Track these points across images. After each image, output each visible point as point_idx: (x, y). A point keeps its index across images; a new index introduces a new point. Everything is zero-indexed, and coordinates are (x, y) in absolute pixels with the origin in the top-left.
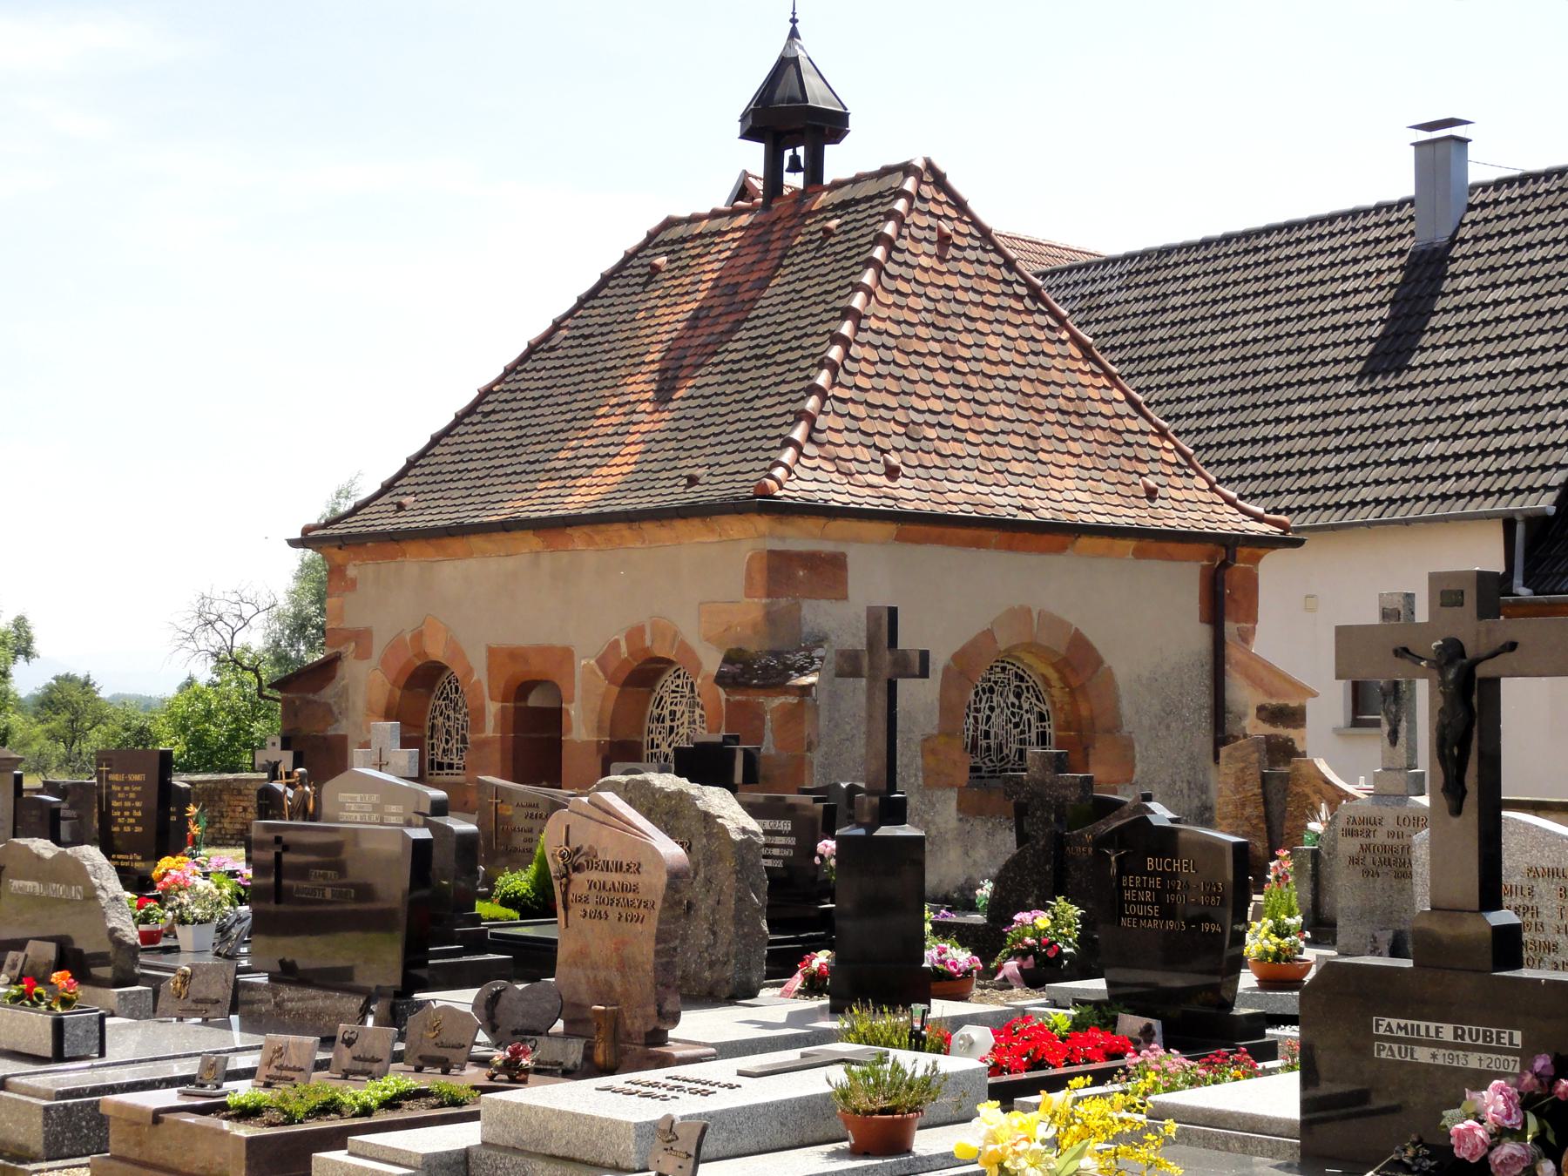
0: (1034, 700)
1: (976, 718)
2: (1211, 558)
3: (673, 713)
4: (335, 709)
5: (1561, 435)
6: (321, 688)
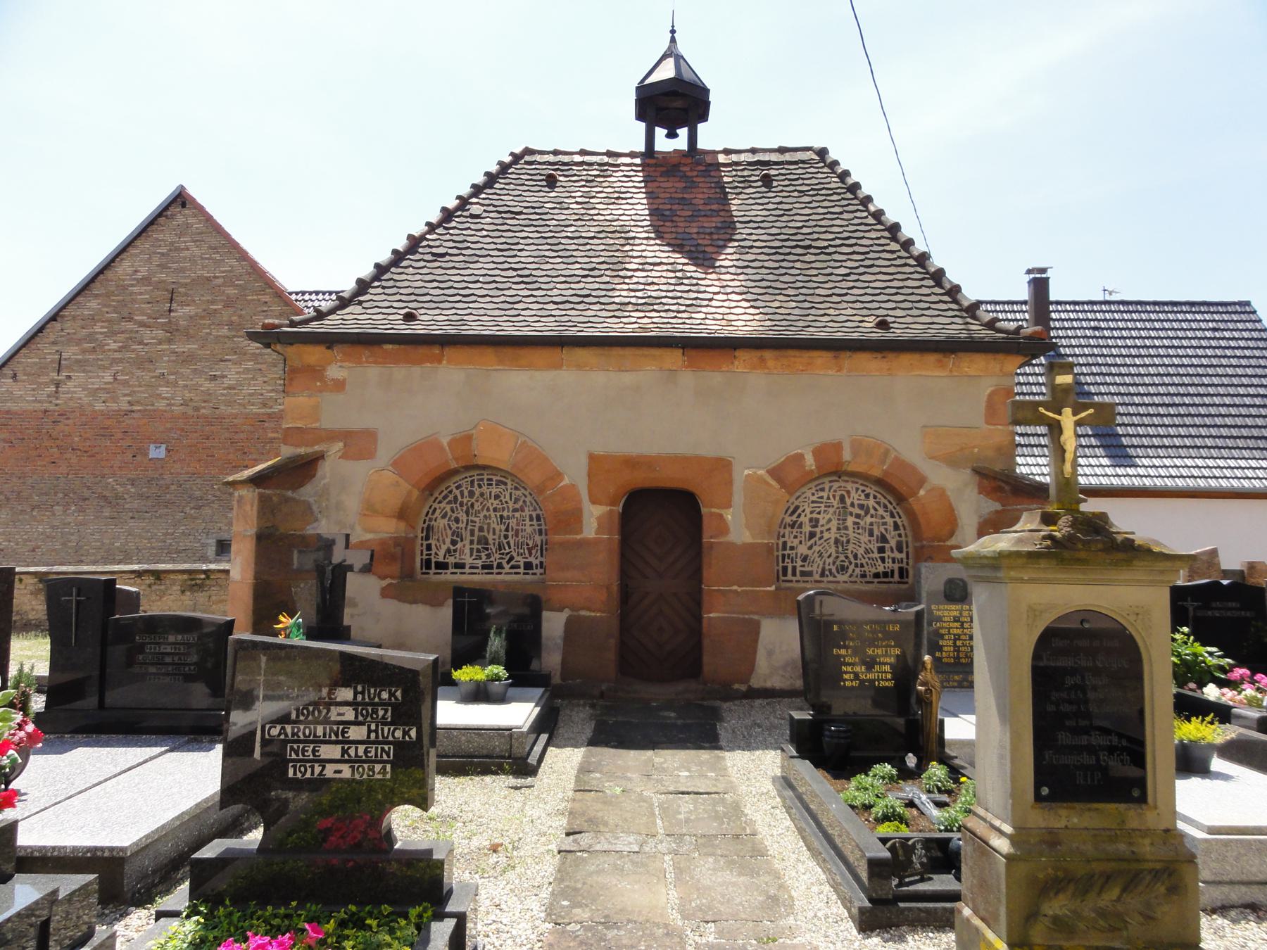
3: (814, 523)
4: (315, 508)
5: (1265, 381)
6: (301, 485)
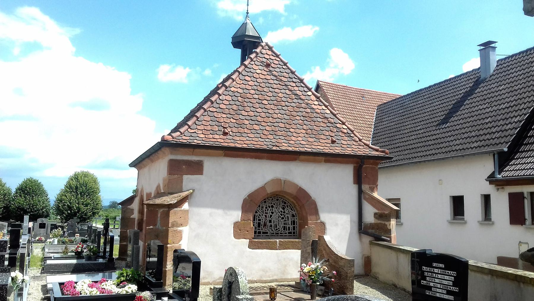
0: (290, 210)
1: (266, 216)
2: (357, 163)
